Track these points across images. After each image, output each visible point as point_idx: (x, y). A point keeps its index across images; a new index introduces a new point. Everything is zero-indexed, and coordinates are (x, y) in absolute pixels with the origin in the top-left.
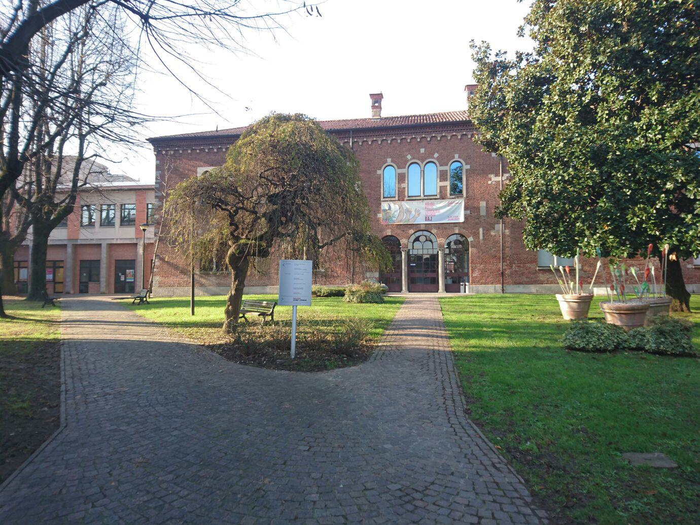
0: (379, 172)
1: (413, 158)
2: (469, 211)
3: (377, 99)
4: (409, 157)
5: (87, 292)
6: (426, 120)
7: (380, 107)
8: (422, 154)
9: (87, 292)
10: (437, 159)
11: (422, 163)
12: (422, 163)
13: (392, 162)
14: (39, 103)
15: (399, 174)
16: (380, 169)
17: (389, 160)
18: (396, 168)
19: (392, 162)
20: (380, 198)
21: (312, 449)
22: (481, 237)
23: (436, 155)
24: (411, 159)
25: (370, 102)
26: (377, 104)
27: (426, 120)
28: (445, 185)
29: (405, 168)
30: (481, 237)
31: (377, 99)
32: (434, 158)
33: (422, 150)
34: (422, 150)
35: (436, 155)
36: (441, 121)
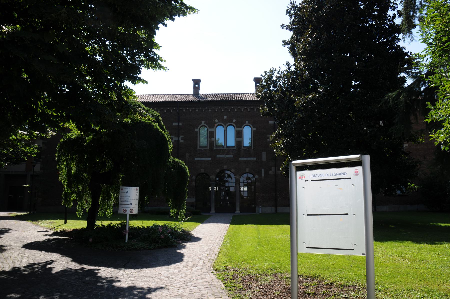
0: (196, 130)
1: (220, 122)
2: (255, 158)
3: (197, 83)
4: (217, 121)
5: (377, 239)
6: (244, 98)
7: (199, 88)
8: (225, 119)
9: (377, 239)
10: (235, 123)
11: (225, 125)
12: (225, 125)
13: (205, 124)
14: (374, 32)
15: (210, 132)
16: (197, 128)
17: (203, 122)
18: (252, 127)
19: (205, 124)
20: (197, 147)
21: (129, 276)
22: (263, 176)
23: (234, 121)
24: (218, 123)
25: (192, 84)
26: (197, 86)
27: (244, 98)
28: (237, 139)
29: (214, 128)
30: (263, 176)
31: (197, 83)
32: (233, 123)
33: (225, 117)
34: (225, 117)
35: (234, 121)
36: (238, 99)
